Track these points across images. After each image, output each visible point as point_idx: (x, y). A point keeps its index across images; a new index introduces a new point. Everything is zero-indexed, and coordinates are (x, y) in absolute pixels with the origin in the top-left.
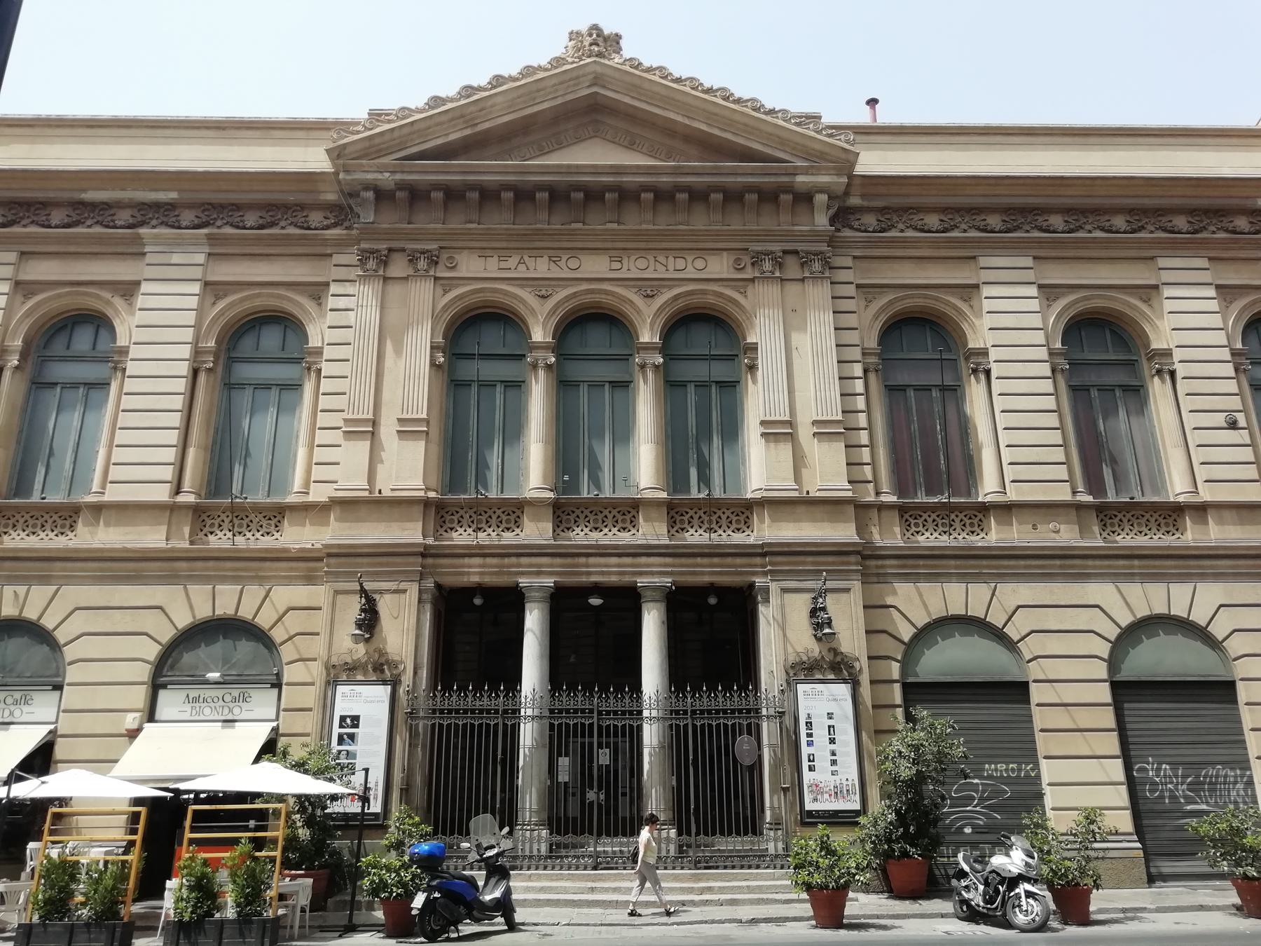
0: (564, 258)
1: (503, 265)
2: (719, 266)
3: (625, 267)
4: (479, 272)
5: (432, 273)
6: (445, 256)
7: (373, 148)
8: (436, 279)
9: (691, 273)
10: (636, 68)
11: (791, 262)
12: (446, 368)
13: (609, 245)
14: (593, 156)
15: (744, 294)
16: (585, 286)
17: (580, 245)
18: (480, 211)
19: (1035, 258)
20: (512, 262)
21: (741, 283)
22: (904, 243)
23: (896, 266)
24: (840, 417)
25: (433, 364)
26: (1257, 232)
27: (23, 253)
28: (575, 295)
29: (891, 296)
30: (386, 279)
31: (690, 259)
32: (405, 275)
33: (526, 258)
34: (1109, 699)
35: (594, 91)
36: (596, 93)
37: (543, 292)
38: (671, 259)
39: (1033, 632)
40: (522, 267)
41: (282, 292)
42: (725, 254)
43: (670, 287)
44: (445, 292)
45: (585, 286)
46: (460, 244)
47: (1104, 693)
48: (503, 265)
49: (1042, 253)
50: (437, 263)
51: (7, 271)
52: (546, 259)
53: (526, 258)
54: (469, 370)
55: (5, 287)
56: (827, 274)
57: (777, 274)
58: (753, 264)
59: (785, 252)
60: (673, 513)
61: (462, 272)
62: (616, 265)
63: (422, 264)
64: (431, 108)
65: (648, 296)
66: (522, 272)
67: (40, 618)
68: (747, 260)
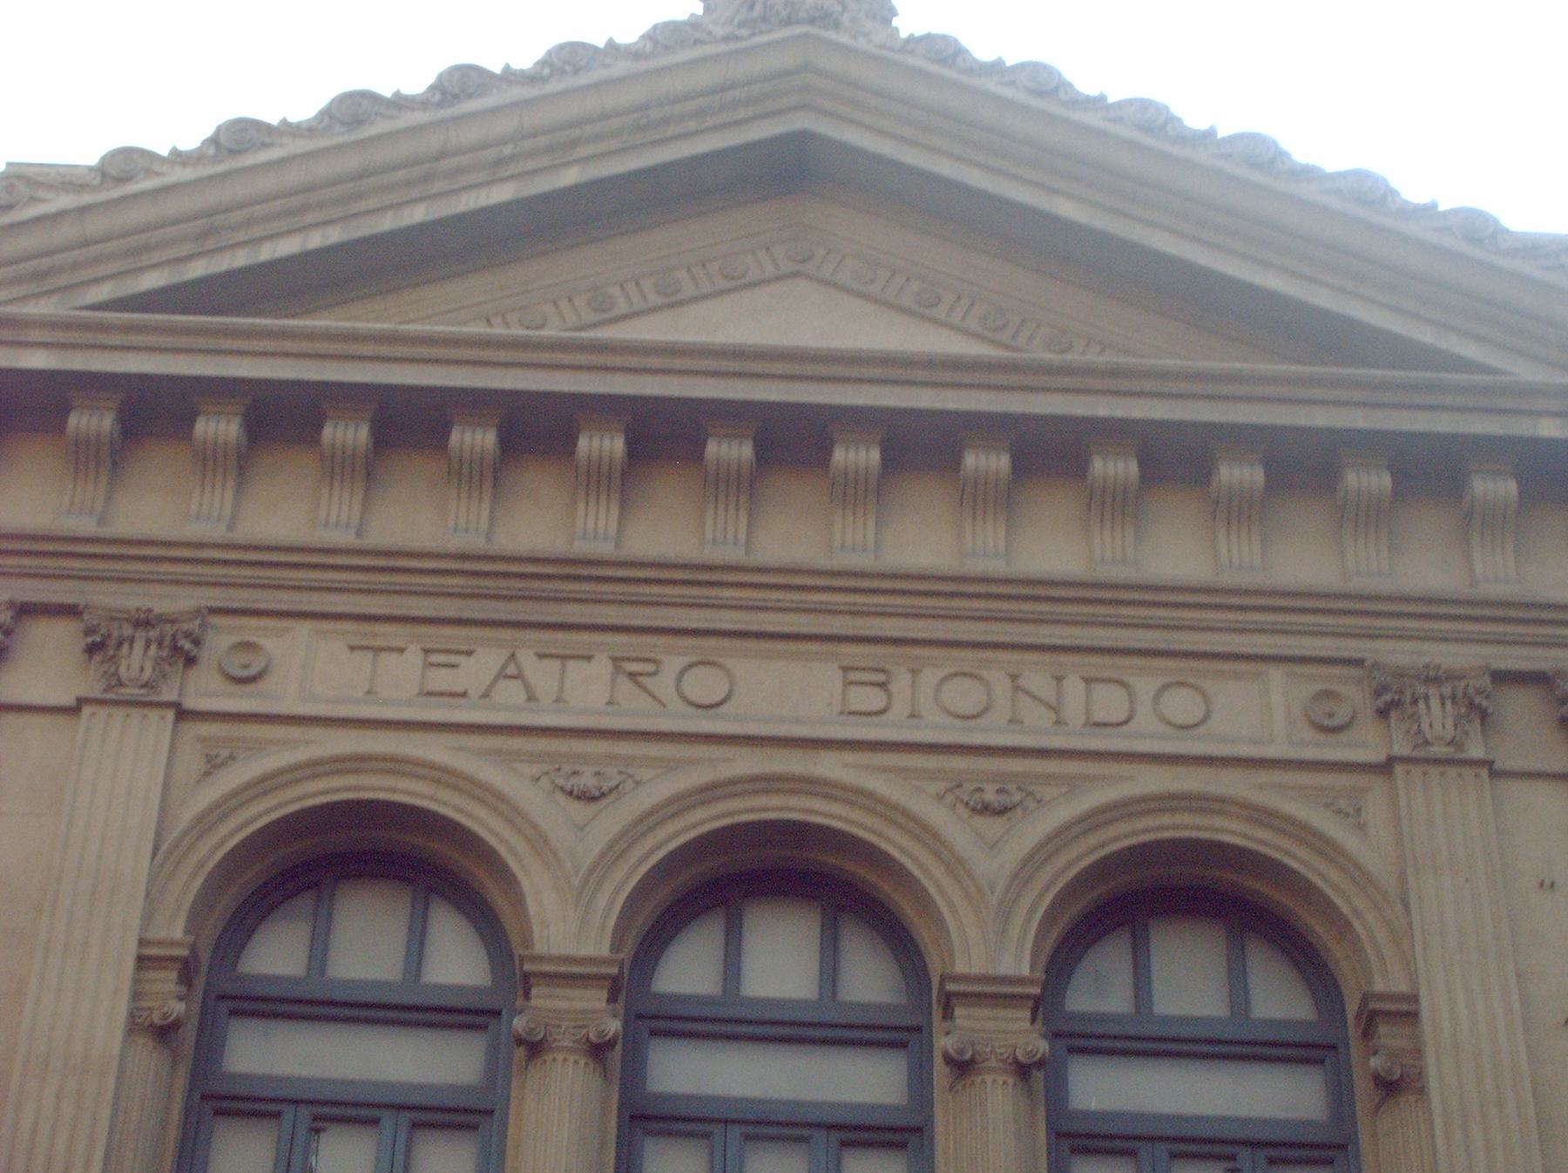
0: (673, 664)
1: (441, 679)
2: (1255, 713)
3: (900, 709)
4: (341, 700)
5: (169, 695)
6: (220, 640)
9: (1147, 735)
10: (943, 61)
11: (1518, 707)
12: (189, 1034)
15: (1354, 816)
16: (745, 763)
18: (240, 486)
20: (481, 665)
21: (1342, 780)
23: (27, 352)
25: (137, 1025)
28: (709, 792)
31: (1145, 686)
32: (68, 700)
33: (527, 659)
36: (803, 137)
37: (587, 781)
38: (1074, 687)
40: (511, 692)
42: (1276, 674)
43: (1072, 784)
44: (213, 765)
45: (745, 763)
48: (441, 679)
50: (191, 661)
52: (601, 667)
53: (527, 659)
54: (260, 1053)
57: (1476, 751)
58: (1383, 713)
59: (1502, 678)
63: (137, 661)
65: (985, 810)
66: (508, 705)
68: (1355, 696)
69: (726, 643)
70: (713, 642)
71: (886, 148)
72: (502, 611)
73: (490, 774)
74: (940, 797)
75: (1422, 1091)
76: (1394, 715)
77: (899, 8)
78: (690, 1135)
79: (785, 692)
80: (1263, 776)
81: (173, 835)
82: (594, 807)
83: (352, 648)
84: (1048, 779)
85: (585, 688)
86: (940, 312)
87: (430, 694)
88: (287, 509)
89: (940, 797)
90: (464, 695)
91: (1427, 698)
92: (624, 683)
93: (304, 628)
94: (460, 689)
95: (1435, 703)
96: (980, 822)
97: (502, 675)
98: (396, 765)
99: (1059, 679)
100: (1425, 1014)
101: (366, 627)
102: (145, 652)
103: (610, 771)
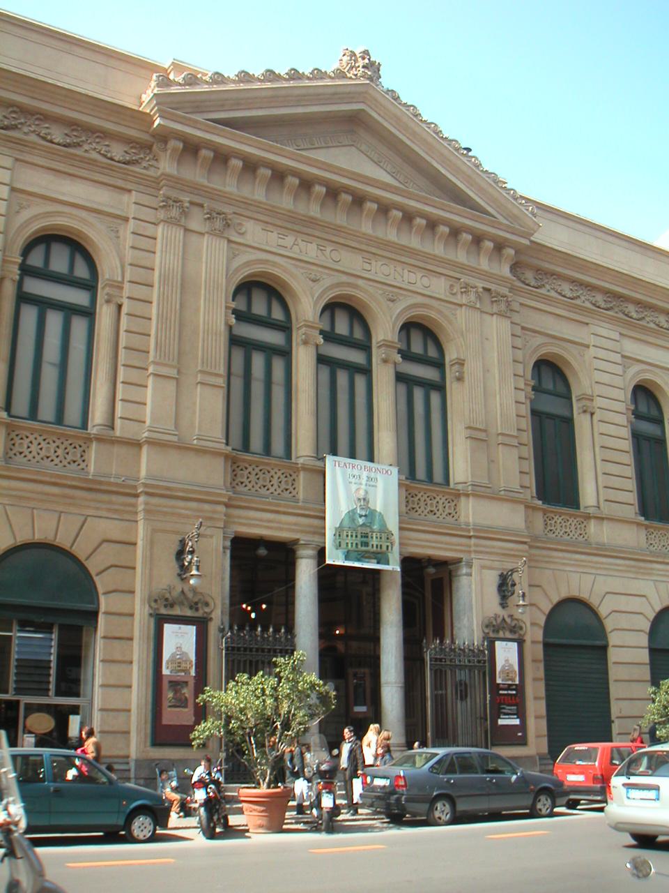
0: (329, 249)
1: (281, 242)
2: (439, 287)
7: (197, 104)
8: (229, 241)
13: (364, 247)
14: (350, 162)
17: (342, 241)
19: (621, 334)
20: (289, 240)
22: (547, 299)
24: (515, 434)
26: (668, 330)
27: (17, 160)
28: (338, 285)
29: (540, 340)
30: (186, 230)
34: (647, 660)
35: (351, 111)
38: (406, 271)
39: (641, 613)
41: (84, 214)
45: (344, 278)
46: (249, 214)
47: (644, 656)
49: (624, 332)
51: (5, 176)
52: (314, 246)
53: (299, 241)
55: (4, 192)
56: (508, 315)
57: (478, 306)
60: (235, 466)
61: (248, 239)
62: (367, 266)
64: (240, 81)
67: (646, 648)
69: (341, 246)
70: (338, 245)
71: (379, 119)
72: (393, 256)
73: (371, 290)
74: (381, 295)
75: (463, 381)
76: (464, 295)
77: (382, 77)
78: (261, 351)
79: (351, 262)
80: (439, 302)
81: (231, 272)
82: (315, 283)
83: (263, 229)
84: (402, 295)
85: (310, 251)
86: (381, 164)
87: (279, 246)
88: (257, 192)
89: (381, 295)
90: (286, 247)
91: (173, 205)
92: (319, 251)
93: (252, 221)
94: (285, 246)
95: (175, 207)
96: (389, 302)
97: (294, 244)
98: (275, 264)
99: (403, 270)
100: (466, 365)
101: (266, 225)
102: (221, 223)
103: (318, 274)
